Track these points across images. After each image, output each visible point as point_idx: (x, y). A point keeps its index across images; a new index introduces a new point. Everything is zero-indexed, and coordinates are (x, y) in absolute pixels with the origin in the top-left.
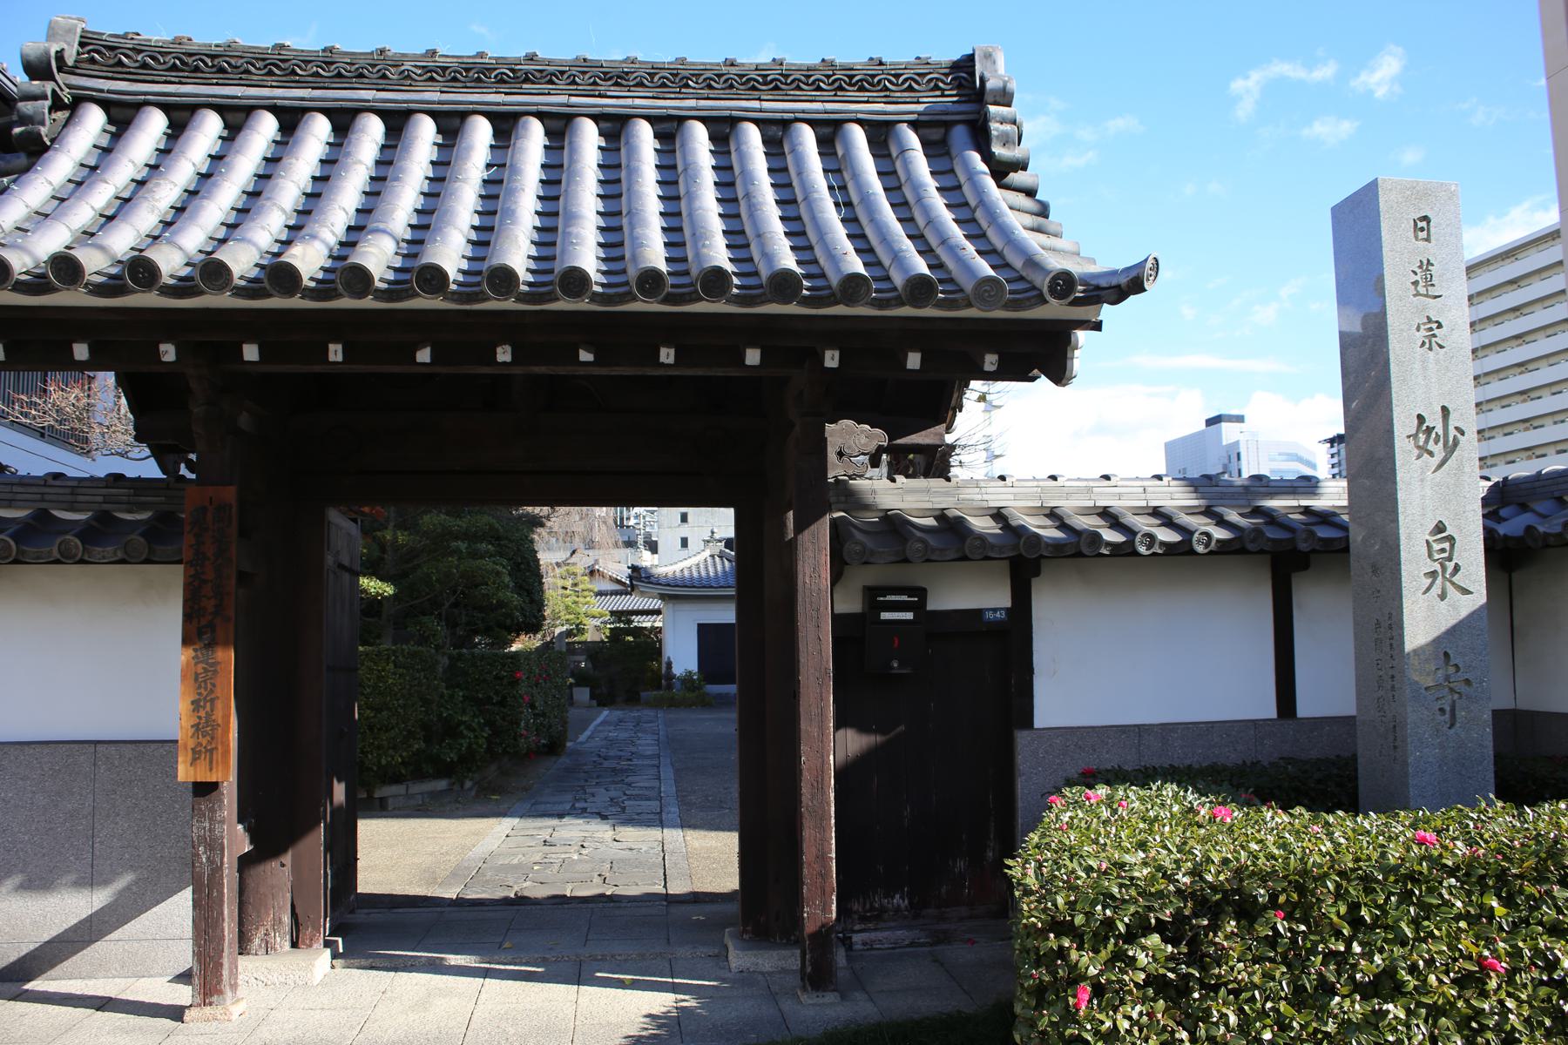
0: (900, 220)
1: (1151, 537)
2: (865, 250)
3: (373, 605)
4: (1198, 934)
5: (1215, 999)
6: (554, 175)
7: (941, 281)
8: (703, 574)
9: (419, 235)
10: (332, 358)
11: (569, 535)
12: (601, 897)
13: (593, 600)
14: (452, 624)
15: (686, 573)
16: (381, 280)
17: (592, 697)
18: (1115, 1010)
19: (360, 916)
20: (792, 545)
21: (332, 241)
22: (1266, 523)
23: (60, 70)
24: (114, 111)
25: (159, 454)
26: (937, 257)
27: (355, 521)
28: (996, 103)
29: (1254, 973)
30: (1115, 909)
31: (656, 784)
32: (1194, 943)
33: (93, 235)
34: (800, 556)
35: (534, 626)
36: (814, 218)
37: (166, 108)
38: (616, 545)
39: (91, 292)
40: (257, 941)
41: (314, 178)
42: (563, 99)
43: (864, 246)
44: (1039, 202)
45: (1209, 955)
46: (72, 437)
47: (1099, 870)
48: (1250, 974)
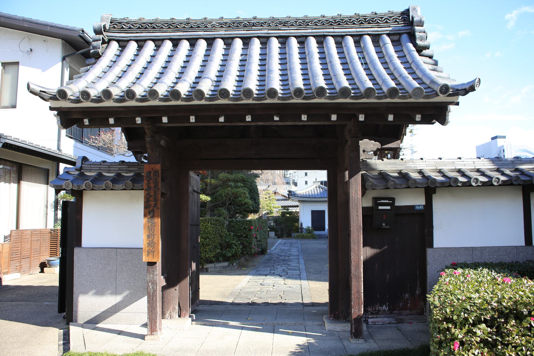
0: (384, 68)
1: (477, 179)
2: (373, 79)
3: (204, 204)
4: (500, 325)
5: (507, 349)
6: (264, 57)
7: (400, 89)
8: (313, 193)
9: (219, 79)
10: (191, 121)
11: (267, 181)
12: (281, 303)
13: (275, 202)
14: (229, 210)
15: (307, 193)
16: (207, 94)
17: (275, 235)
18: (469, 351)
19: (200, 307)
20: (347, 184)
21: (191, 82)
22: (520, 174)
23: (104, 31)
24: (121, 43)
25: (135, 154)
26: (398, 81)
27: (198, 176)
28: (418, 26)
29: (522, 340)
30: (469, 314)
31: (298, 265)
32: (498, 328)
33: (115, 83)
34: (351, 187)
35: (256, 211)
36: (354, 69)
37: (137, 41)
38: (283, 184)
39: (71, 102)
40: (167, 315)
41: (184, 62)
42: (266, 31)
43: (372, 78)
44: (434, 60)
45: (504, 333)
46: (107, 150)
47: (462, 300)
48: (521, 341)
